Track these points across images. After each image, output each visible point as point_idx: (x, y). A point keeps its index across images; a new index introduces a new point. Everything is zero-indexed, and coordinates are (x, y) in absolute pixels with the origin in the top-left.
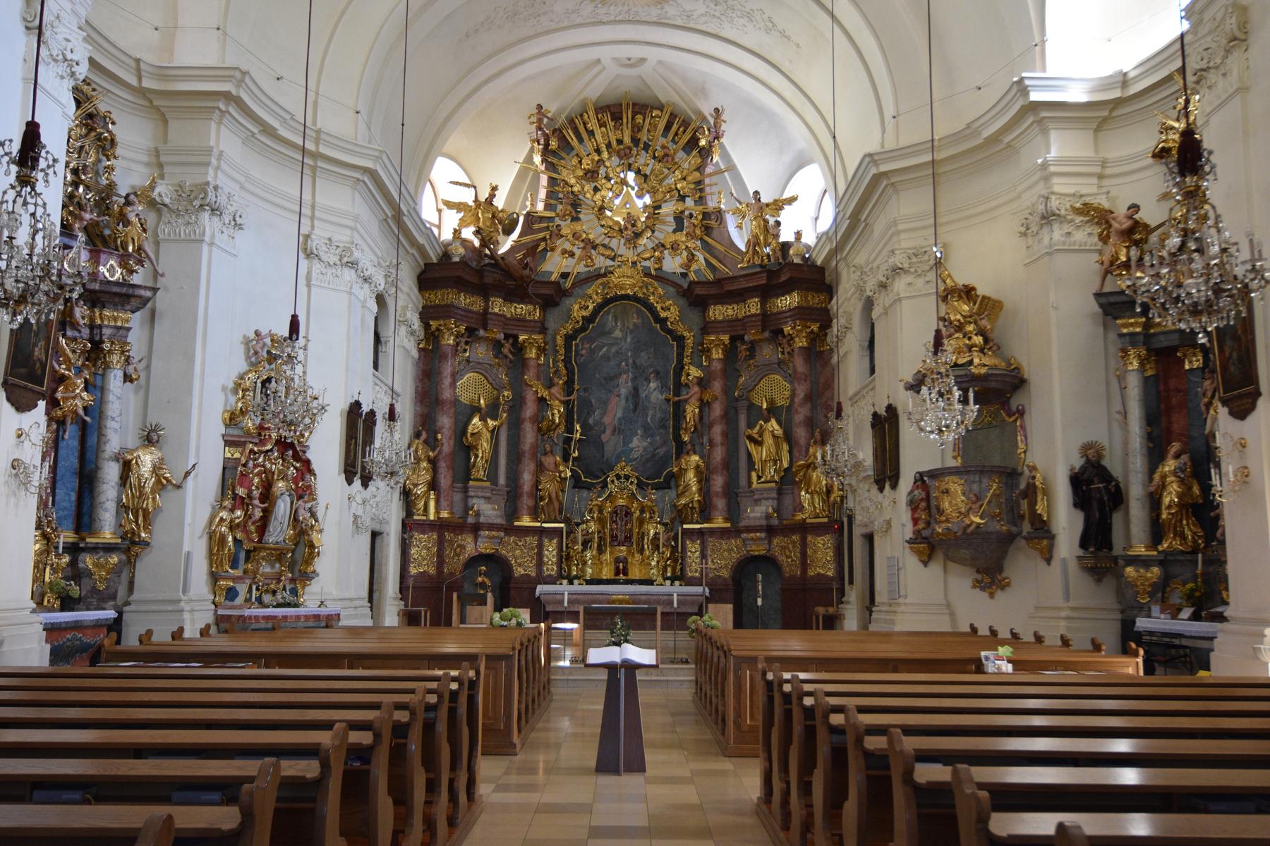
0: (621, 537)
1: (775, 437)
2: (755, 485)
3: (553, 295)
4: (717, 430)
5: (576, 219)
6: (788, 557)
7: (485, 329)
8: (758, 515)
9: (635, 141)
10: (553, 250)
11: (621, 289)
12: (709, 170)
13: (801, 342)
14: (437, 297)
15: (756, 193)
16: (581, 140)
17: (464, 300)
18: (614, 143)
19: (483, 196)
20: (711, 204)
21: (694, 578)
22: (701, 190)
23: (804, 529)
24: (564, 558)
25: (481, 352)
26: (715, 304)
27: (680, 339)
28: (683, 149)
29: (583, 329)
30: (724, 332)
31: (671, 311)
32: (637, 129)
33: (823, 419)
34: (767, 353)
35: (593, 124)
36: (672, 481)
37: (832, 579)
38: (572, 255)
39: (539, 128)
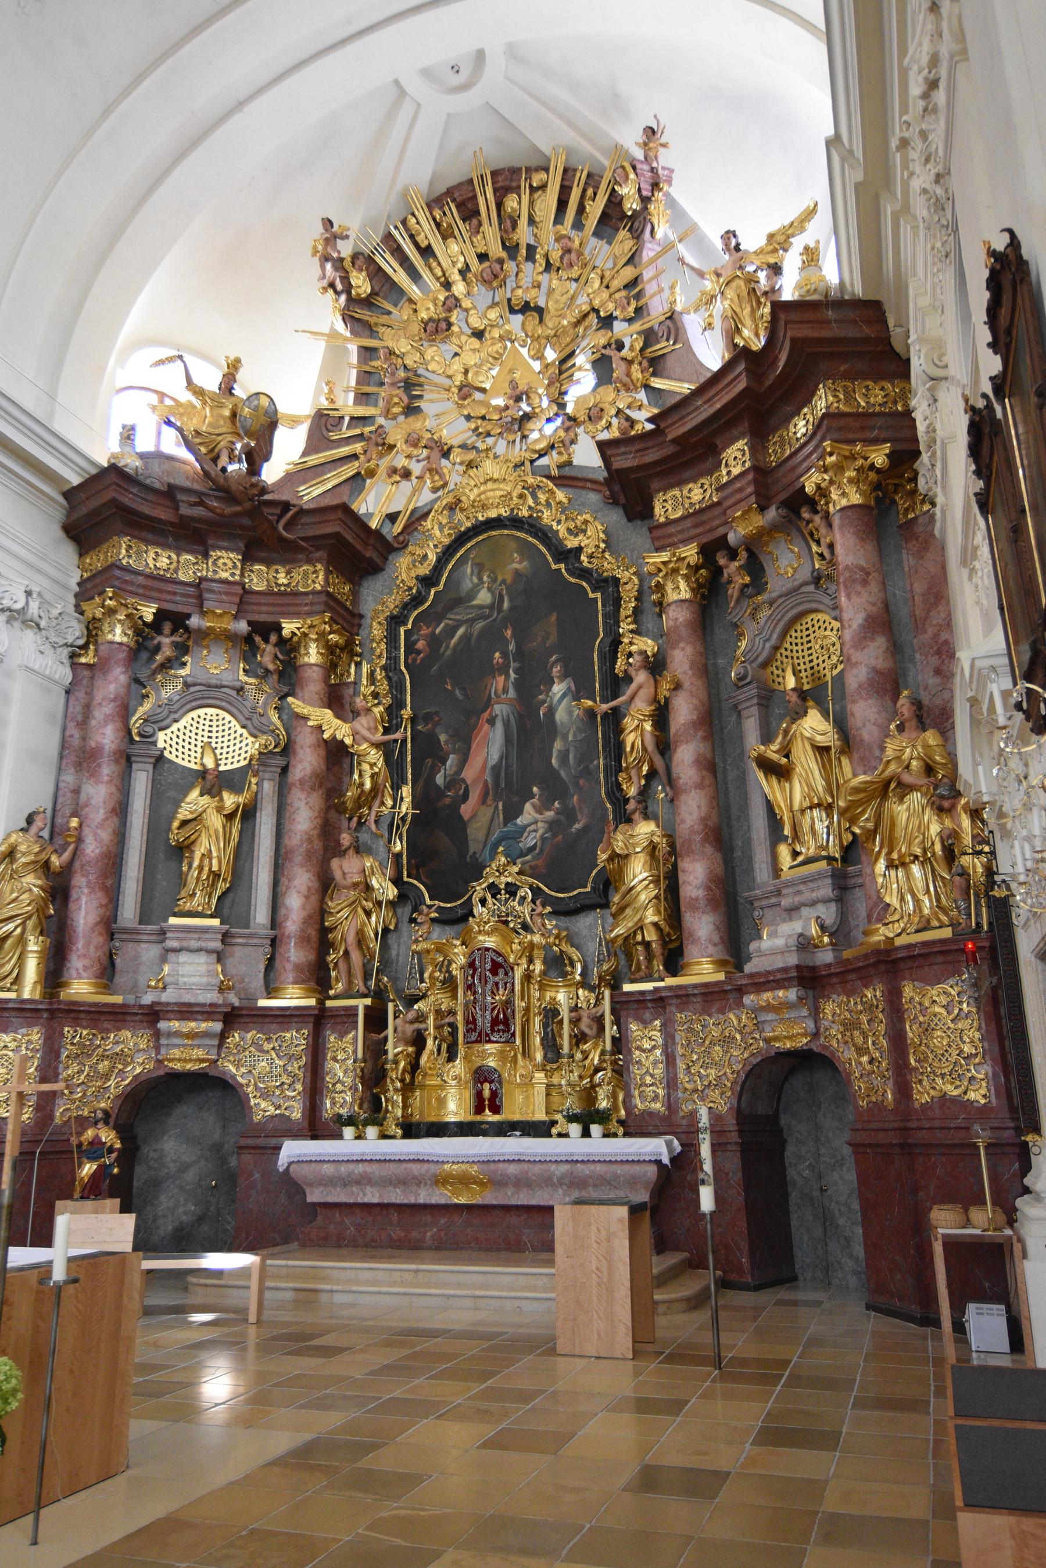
0: (484, 1021)
1: (822, 751)
2: (787, 874)
3: (355, 550)
4: (686, 757)
5: (411, 411)
6: (861, 1051)
7: (203, 614)
8: (780, 942)
9: (511, 249)
10: (371, 473)
11: (484, 507)
12: (649, 251)
13: (846, 496)
14: (96, 561)
15: (730, 235)
16: (414, 275)
17: (158, 559)
18: (475, 265)
19: (210, 379)
20: (657, 309)
21: (651, 1114)
22: (638, 296)
23: (892, 965)
24: (373, 1075)
25: (215, 665)
26: (665, 489)
27: (610, 585)
28: (597, 234)
29: (417, 600)
30: (685, 542)
31: (588, 530)
32: (508, 222)
33: (933, 681)
34: (788, 564)
35: (428, 234)
36: (606, 890)
37: (983, 1112)
38: (406, 474)
39: (326, 258)
